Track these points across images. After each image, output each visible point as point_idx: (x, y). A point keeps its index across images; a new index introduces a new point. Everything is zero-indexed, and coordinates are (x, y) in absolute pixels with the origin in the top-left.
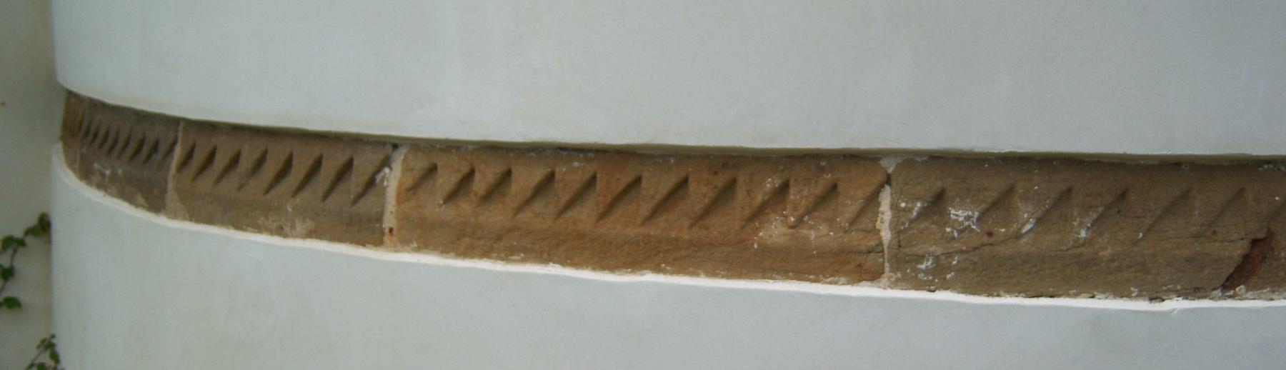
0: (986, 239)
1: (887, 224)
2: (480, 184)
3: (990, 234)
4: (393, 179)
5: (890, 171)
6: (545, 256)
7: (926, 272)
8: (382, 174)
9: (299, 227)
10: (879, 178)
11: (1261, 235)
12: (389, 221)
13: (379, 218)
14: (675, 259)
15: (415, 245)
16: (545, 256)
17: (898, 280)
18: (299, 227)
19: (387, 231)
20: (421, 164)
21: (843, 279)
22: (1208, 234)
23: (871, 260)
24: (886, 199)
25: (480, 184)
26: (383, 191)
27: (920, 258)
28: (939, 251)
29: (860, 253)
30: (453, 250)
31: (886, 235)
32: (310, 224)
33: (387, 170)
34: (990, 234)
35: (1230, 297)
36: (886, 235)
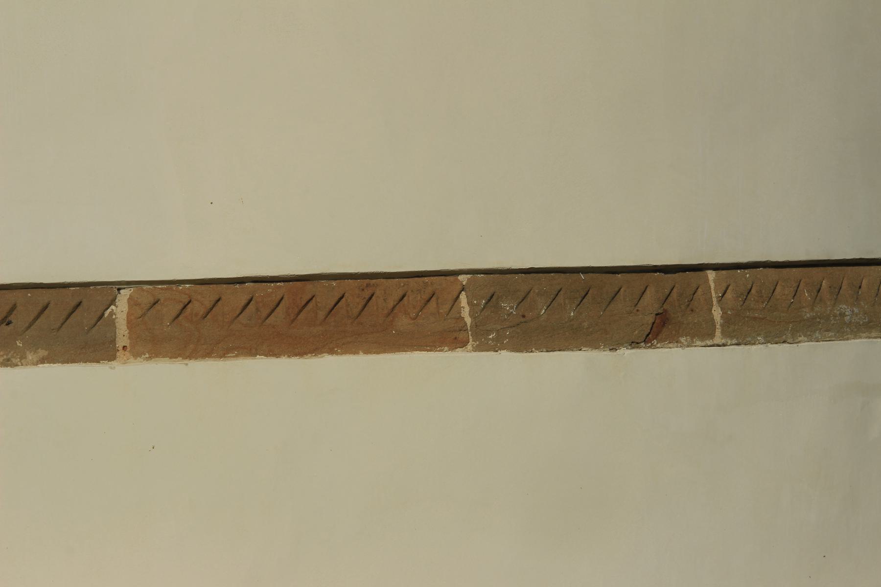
0: (523, 320)
1: (467, 313)
2: (197, 308)
3: (524, 316)
4: (121, 309)
5: (464, 283)
6: (254, 351)
7: (493, 339)
8: (109, 310)
9: (30, 356)
10: (459, 287)
11: (660, 311)
12: (120, 344)
13: (113, 341)
14: (343, 344)
15: (147, 356)
16: (254, 351)
17: (477, 346)
18: (30, 356)
19: (121, 348)
20: (146, 300)
21: (446, 348)
22: (635, 311)
23: (461, 335)
24: (463, 297)
25: (197, 308)
26: (112, 323)
27: (489, 332)
28: (499, 327)
29: (455, 331)
30: (179, 355)
31: (468, 320)
32: (42, 353)
33: (113, 307)
34: (524, 316)
35: (649, 347)
36: (468, 320)
